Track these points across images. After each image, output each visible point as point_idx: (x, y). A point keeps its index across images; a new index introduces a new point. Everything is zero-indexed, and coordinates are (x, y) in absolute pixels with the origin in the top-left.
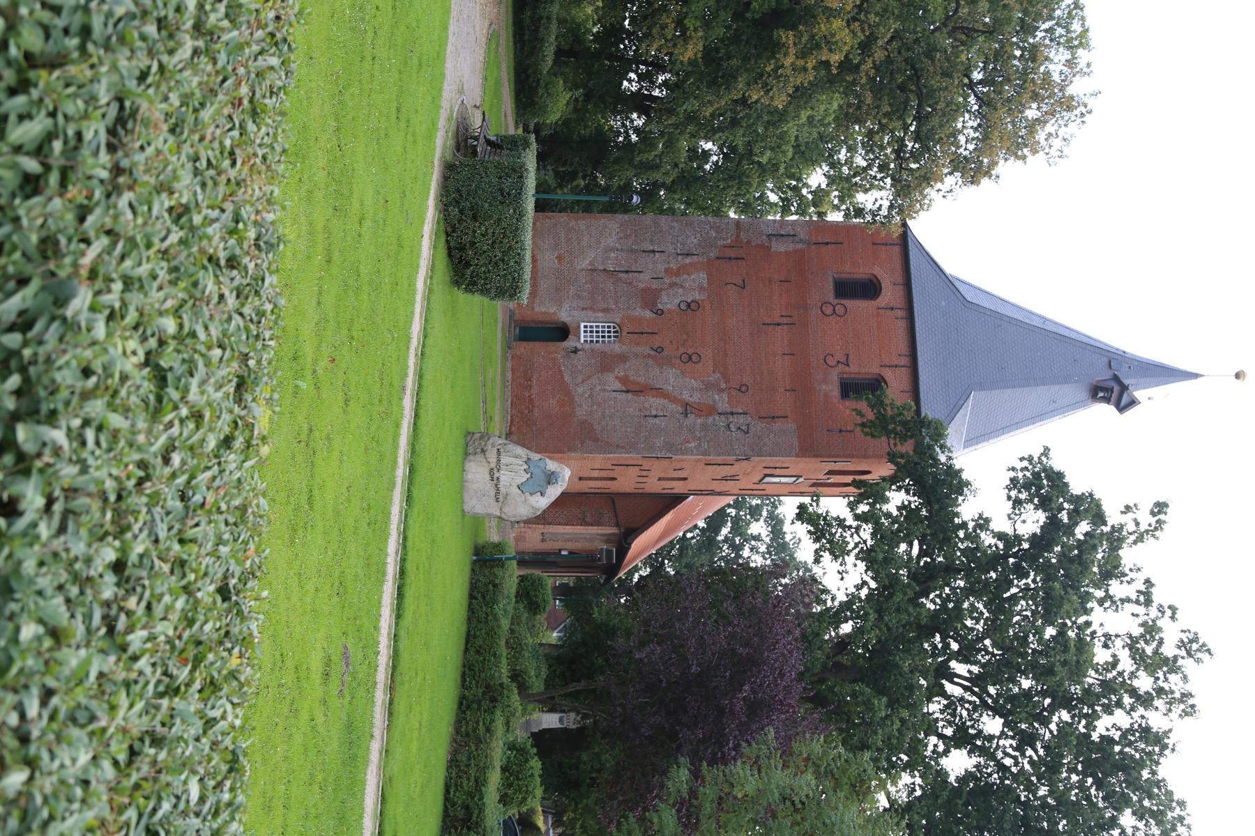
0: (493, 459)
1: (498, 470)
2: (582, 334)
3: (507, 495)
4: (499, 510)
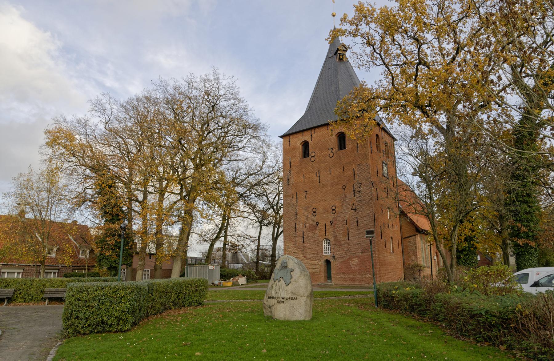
0: (274, 301)
1: (278, 298)
2: (328, 254)
3: (292, 293)
4: (303, 298)
